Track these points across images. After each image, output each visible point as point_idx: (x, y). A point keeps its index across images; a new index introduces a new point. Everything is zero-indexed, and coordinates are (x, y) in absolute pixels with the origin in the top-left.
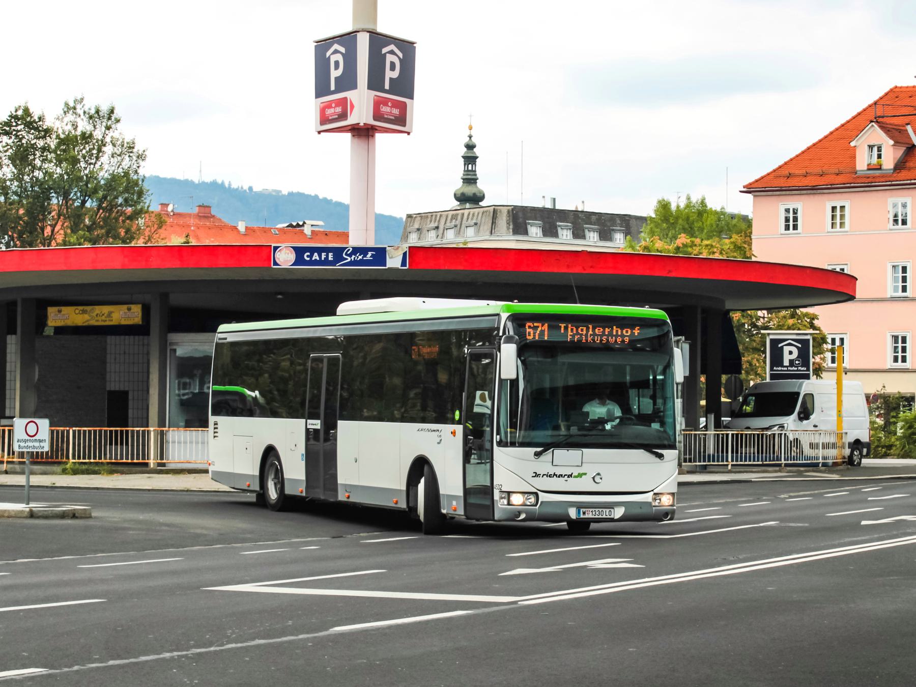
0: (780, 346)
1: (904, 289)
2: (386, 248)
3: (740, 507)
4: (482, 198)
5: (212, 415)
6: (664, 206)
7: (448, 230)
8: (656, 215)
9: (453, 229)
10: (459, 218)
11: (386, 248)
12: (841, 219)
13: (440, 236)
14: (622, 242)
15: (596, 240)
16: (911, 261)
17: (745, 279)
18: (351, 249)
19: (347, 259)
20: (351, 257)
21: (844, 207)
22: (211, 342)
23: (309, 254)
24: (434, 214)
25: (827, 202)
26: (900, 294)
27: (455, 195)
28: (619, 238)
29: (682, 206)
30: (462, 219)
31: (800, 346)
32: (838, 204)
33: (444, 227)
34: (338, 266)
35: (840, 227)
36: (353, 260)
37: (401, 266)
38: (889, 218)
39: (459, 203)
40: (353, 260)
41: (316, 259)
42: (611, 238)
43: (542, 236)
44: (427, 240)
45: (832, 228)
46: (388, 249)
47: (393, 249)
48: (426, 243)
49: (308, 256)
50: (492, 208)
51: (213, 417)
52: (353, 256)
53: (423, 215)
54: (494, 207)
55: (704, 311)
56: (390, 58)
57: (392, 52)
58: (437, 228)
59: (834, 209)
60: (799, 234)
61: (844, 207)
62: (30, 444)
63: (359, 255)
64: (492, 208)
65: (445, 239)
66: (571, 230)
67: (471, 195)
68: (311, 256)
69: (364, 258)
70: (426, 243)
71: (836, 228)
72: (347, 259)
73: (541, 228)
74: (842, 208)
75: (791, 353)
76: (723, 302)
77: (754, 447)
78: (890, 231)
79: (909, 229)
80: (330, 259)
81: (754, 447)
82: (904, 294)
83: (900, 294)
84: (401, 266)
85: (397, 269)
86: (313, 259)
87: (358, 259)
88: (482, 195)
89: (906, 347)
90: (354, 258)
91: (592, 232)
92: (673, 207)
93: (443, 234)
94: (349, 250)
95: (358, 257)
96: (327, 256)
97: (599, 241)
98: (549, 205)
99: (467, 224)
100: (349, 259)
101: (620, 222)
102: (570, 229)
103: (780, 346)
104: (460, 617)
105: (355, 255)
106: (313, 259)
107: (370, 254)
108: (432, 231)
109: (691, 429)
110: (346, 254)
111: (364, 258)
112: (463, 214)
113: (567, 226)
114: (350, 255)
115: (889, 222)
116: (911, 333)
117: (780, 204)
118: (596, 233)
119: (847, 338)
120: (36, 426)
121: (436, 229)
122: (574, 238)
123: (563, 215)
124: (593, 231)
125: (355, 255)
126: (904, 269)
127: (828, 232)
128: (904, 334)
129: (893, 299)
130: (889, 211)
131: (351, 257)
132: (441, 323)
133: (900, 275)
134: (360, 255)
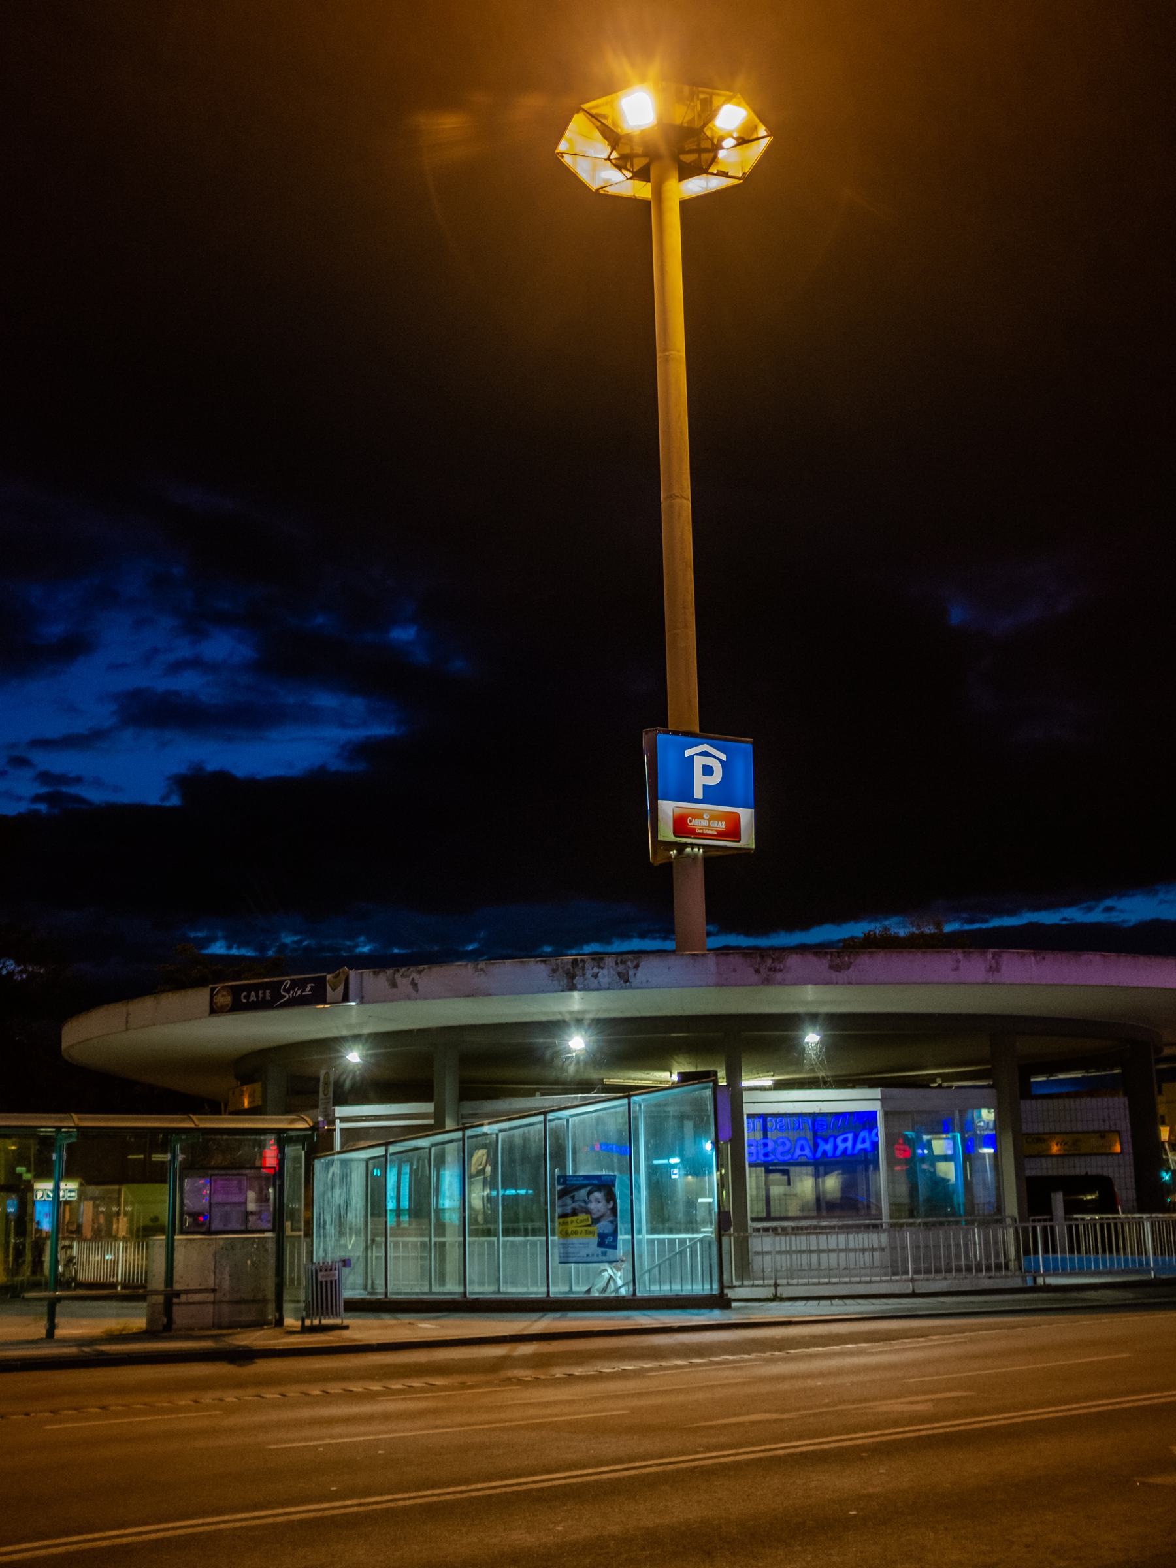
0: (688, 753)
3: (421, 1328)
5: (876, 1112)
17: (691, 575)
18: (289, 983)
19: (285, 996)
20: (289, 993)
23: (245, 994)
31: (723, 757)
41: (253, 1000)
49: (245, 997)
51: (874, 1110)
52: (292, 992)
56: (699, 763)
57: (705, 754)
68: (247, 997)
75: (708, 771)
77: (138, 1265)
80: (268, 998)
81: (138, 1265)
86: (250, 1000)
96: (264, 994)
103: (688, 753)
104: (683, 1036)
105: (294, 990)
106: (250, 1000)
109: (1045, 1217)
110: (285, 990)
114: (288, 991)
125: (294, 990)
131: (289, 993)
132: (728, 1262)
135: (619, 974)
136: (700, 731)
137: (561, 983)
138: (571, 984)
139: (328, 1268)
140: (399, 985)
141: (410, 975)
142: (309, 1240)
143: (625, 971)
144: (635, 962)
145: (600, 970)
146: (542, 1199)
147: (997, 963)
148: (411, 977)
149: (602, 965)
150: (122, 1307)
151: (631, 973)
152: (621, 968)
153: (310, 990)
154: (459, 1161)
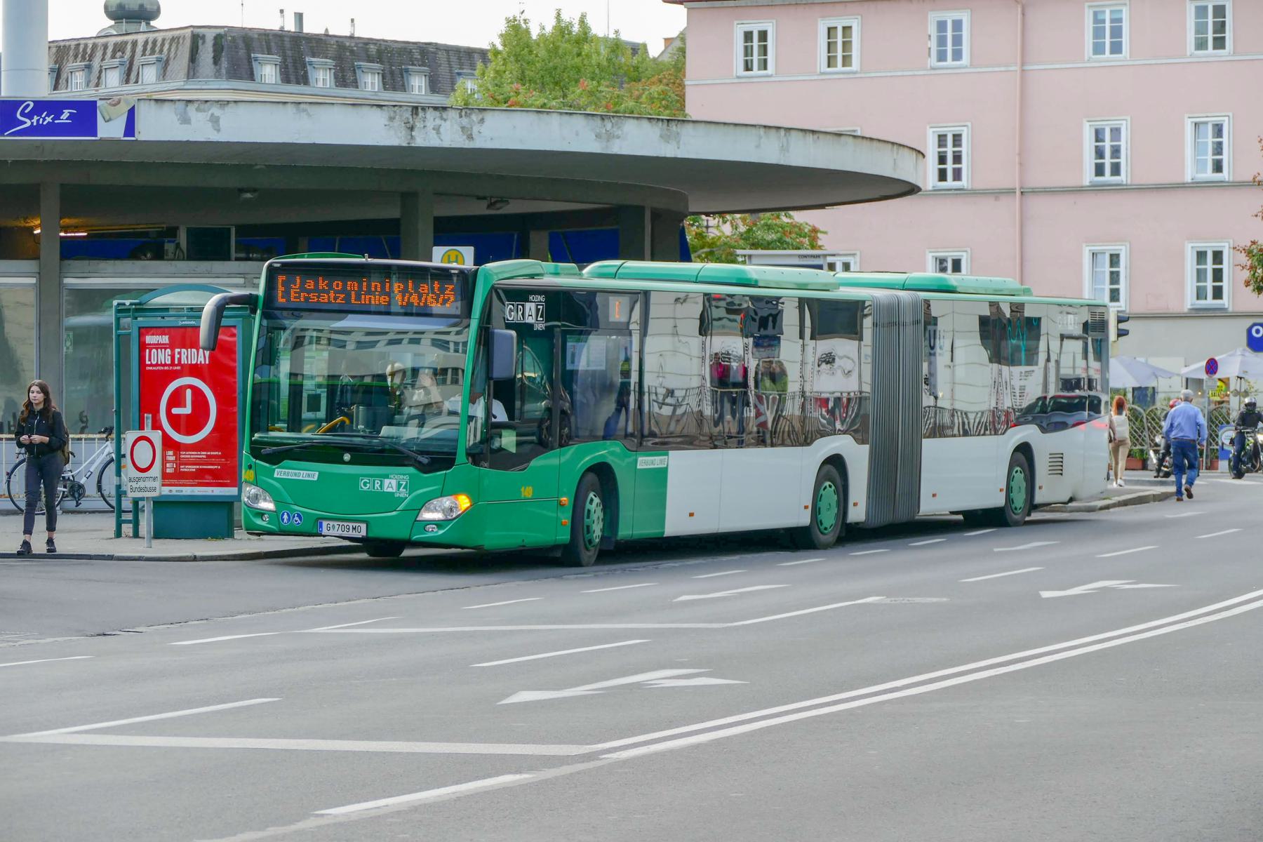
1: (1218, 167)
2: (96, 102)
4: (155, 13)
6: (516, 32)
7: (108, 71)
8: (505, 45)
9: (118, 69)
10: (129, 47)
11: (96, 102)
12: (844, 51)
13: (94, 81)
14: (423, 93)
15: (376, 90)
16: (969, 124)
18: (32, 105)
20: (31, 118)
21: (850, 28)
22: (257, 278)
24: (82, 42)
25: (819, 19)
26: (1209, 175)
27: (106, 7)
28: (417, 85)
29: (549, 29)
30: (133, 51)
32: (755, 28)
33: (101, 66)
34: (7, 135)
35: (844, 65)
36: (35, 124)
37: (124, 136)
38: (930, 49)
39: (112, 22)
40: (35, 124)
42: (403, 85)
43: (280, 82)
44: (69, 90)
45: (829, 66)
46: (99, 103)
47: (110, 104)
48: (67, 95)
50: (189, 31)
52: (36, 118)
53: (62, 44)
54: (192, 29)
55: (656, 215)
58: (89, 67)
59: (748, 36)
60: (771, 76)
61: (850, 28)
62: (141, 484)
63: (47, 115)
64: (189, 31)
65: (103, 87)
66: (333, 71)
67: (136, 8)
69: (56, 121)
70: (67, 95)
71: (836, 66)
72: (25, 123)
73: (278, 67)
74: (847, 29)
76: (685, 200)
78: (933, 72)
79: (966, 67)
82: (1218, 176)
83: (1209, 175)
84: (124, 136)
85: (119, 141)
87: (45, 123)
88: (155, 7)
89: (1221, 270)
90: (38, 121)
91: (370, 75)
92: (535, 33)
93: (99, 78)
94: (28, 105)
95: (44, 120)
97: (382, 90)
98: (290, 26)
99: (144, 59)
100: (29, 124)
101: (419, 57)
102: (330, 69)
107: (66, 113)
108: (77, 74)
110: (23, 114)
111: (56, 121)
112: (135, 43)
113: (326, 64)
114: (30, 116)
115: (929, 55)
116: (969, 252)
117: (736, 22)
118: (377, 75)
119: (855, 263)
120: (135, 447)
121: (86, 70)
122: (337, 86)
123: (319, 44)
124: (372, 73)
126: (1218, 130)
127: (738, 77)
128: (956, 255)
129: (1096, 189)
130: (930, 36)
131: (31, 118)
133: (1210, 140)
134: (48, 115)
135: (463, 128)
136: (509, 420)
137: (400, 135)
138: (410, 137)
139: (818, 238)
140: (193, 120)
141: (209, 110)
142: (170, 310)
143: (469, 126)
144: (480, 117)
145: (443, 122)
146: (940, 250)
147: (787, 140)
148: (210, 112)
149: (445, 116)
150: (532, 276)
151: (475, 130)
152: (465, 121)
153: (63, 113)
154: (738, 279)
